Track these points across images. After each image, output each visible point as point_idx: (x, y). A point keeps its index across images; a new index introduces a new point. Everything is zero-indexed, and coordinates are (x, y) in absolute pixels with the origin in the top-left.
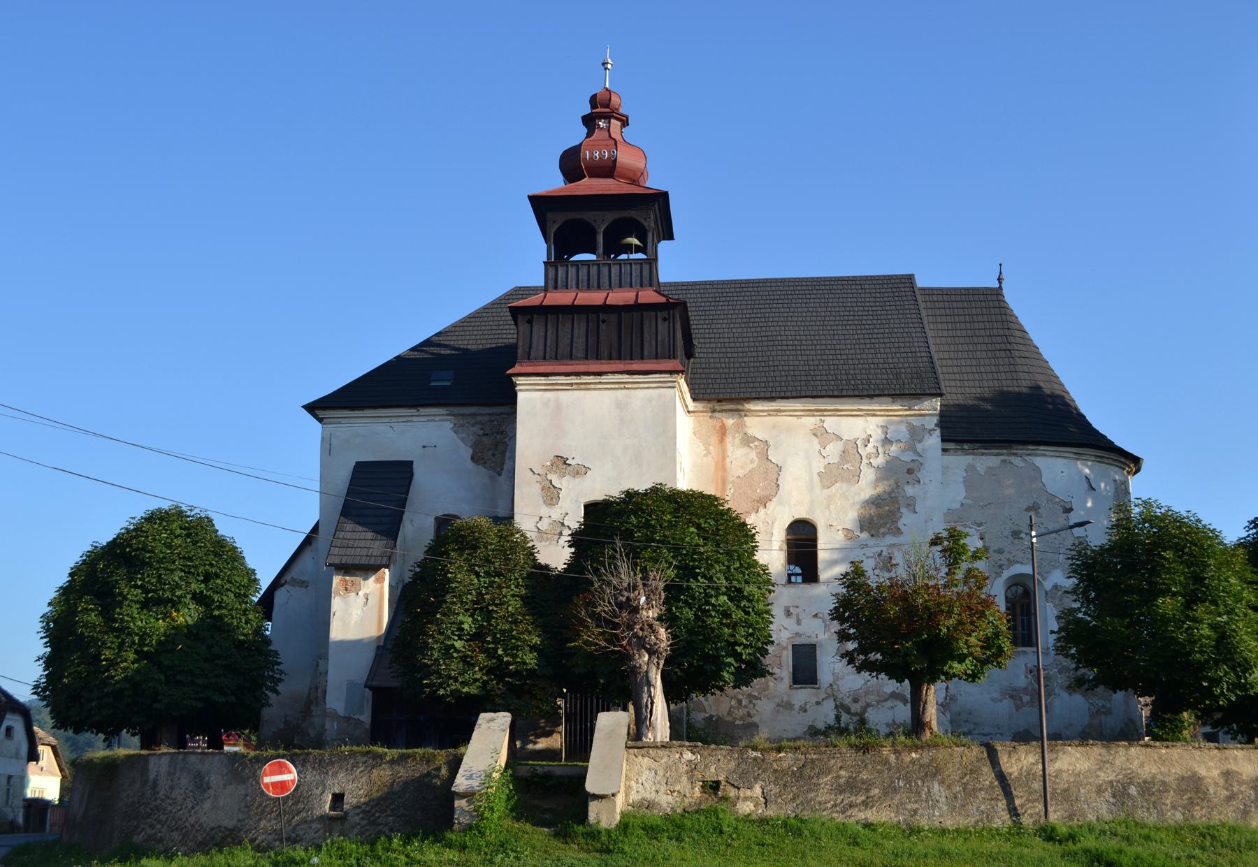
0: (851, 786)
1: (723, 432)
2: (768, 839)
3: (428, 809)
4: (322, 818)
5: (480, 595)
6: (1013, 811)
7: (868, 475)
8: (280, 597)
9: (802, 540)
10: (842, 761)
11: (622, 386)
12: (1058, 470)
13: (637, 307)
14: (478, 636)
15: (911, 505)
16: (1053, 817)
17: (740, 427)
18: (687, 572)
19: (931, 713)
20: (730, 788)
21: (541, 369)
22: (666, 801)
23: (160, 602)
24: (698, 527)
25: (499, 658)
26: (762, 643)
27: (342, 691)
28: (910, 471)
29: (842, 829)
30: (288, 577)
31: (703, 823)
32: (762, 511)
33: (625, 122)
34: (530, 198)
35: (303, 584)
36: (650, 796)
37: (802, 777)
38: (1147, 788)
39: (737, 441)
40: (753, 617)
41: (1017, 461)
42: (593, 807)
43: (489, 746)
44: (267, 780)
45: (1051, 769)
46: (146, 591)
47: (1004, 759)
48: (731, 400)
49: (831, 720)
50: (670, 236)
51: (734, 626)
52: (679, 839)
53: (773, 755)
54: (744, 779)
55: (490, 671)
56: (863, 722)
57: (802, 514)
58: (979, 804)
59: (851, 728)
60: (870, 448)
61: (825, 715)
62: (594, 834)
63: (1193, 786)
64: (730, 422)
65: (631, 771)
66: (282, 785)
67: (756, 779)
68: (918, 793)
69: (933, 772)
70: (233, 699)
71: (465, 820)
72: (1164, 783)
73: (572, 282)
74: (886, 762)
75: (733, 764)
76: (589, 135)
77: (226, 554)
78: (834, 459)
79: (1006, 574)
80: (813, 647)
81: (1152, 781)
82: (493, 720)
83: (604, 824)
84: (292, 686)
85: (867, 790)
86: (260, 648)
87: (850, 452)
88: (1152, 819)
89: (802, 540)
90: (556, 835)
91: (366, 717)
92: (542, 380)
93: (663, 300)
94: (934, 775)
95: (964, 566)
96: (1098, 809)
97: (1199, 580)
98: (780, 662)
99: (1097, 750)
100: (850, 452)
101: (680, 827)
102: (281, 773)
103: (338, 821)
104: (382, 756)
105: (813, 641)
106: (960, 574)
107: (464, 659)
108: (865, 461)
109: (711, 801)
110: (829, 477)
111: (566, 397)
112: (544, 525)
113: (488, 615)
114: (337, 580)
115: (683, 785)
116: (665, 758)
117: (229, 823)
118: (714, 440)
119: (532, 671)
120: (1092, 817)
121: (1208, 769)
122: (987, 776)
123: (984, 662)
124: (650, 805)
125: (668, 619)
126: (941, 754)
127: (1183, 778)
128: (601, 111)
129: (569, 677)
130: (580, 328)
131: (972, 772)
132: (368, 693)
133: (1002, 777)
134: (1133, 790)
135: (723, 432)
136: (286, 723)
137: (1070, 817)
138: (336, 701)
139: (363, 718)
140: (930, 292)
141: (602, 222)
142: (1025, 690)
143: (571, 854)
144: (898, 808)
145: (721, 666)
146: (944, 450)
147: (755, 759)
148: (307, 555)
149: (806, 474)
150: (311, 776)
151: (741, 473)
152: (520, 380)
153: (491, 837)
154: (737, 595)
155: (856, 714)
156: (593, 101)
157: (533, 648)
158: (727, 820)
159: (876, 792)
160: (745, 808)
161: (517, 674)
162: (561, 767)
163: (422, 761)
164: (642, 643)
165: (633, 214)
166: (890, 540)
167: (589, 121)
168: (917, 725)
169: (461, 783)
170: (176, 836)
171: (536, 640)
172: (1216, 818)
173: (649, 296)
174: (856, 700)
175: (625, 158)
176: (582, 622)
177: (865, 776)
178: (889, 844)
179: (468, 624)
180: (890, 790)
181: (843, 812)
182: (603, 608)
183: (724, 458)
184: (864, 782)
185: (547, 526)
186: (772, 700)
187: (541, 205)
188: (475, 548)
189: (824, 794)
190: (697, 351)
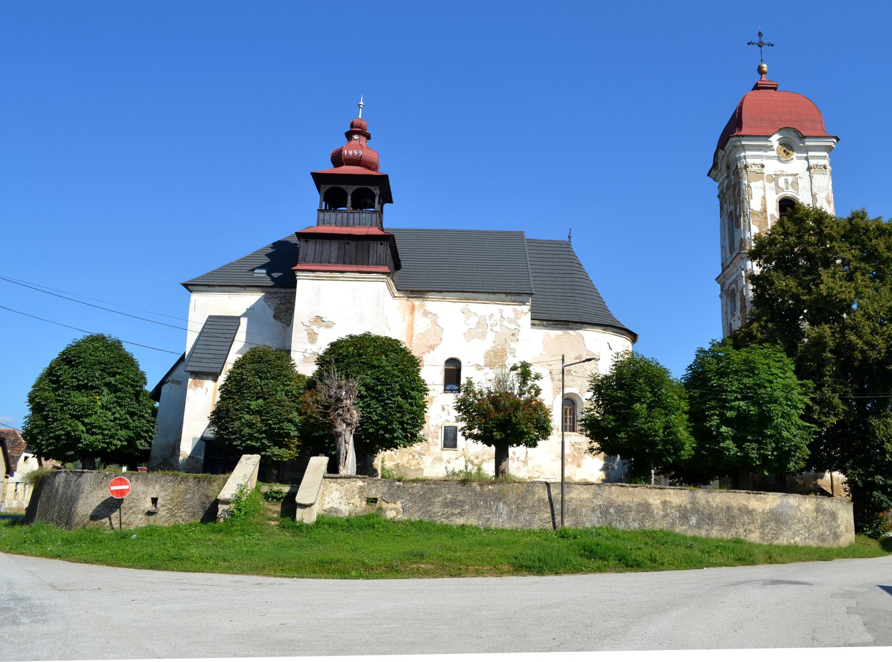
0: (453, 504)
1: (413, 308)
7: (490, 336)
8: (165, 389)
16: (566, 524)
17: (422, 306)
20: (384, 503)
22: (345, 510)
23: (86, 387)
28: (513, 335)
30: (170, 378)
33: (368, 137)
36: (336, 505)
39: (421, 314)
41: (571, 332)
42: (299, 512)
45: (567, 497)
49: (463, 468)
50: (391, 201)
56: (479, 469)
63: (646, 508)
67: (399, 498)
68: (491, 509)
70: (126, 443)
72: (629, 507)
74: (474, 490)
75: (385, 490)
78: (473, 325)
82: (249, 459)
85: (462, 506)
88: (621, 526)
91: (202, 457)
93: (382, 233)
94: (500, 499)
96: (592, 521)
102: (121, 485)
108: (489, 328)
110: (470, 335)
114: (190, 380)
118: (408, 313)
120: (588, 525)
121: (655, 500)
124: (337, 511)
127: (640, 504)
131: (523, 498)
134: (612, 510)
135: (413, 308)
137: (576, 525)
141: (350, 190)
144: (479, 517)
146: (533, 325)
147: (398, 486)
156: (352, 125)
159: (467, 507)
160: (390, 514)
172: (657, 526)
174: (477, 458)
177: (461, 498)
180: (474, 507)
181: (447, 518)
183: (413, 323)
184: (460, 502)
187: (319, 179)
189: (437, 509)
190: (403, 263)
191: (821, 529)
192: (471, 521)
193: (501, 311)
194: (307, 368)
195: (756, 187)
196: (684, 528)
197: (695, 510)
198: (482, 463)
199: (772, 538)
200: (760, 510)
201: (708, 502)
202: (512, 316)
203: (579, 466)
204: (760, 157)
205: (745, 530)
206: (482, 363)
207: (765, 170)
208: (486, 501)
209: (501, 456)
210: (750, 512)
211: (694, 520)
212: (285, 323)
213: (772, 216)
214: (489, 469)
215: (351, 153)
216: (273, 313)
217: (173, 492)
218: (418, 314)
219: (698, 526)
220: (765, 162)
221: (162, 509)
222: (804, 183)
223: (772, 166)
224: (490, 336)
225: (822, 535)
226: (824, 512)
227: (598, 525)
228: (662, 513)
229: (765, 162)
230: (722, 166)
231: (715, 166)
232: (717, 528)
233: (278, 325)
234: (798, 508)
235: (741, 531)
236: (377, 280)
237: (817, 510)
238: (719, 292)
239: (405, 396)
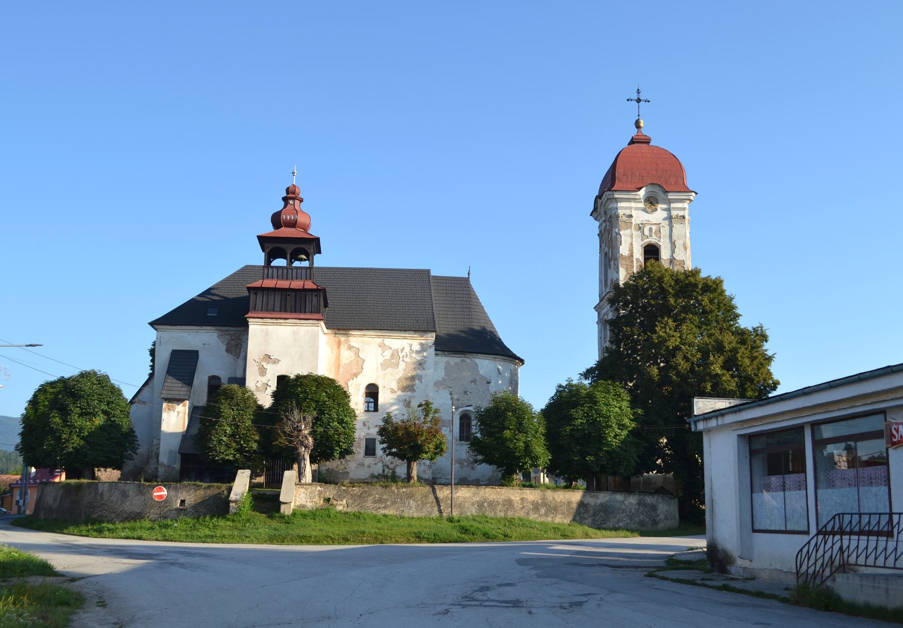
0: (380, 501)
1: (339, 343)
2: (347, 520)
3: (220, 507)
4: (176, 509)
5: (234, 418)
6: (440, 511)
7: (402, 365)
9: (372, 392)
10: (377, 491)
11: (296, 325)
12: (486, 365)
13: (304, 290)
14: (233, 436)
16: (454, 514)
17: (347, 341)
18: (321, 412)
19: (414, 473)
21: (260, 315)
22: (310, 505)
23: (88, 414)
24: (326, 392)
25: (242, 445)
26: (350, 440)
27: (167, 455)
29: (375, 516)
30: (137, 400)
31: (324, 513)
34: (258, 237)
35: (144, 403)
36: (304, 503)
37: (361, 497)
38: (491, 504)
40: (347, 431)
41: (468, 360)
42: (283, 507)
43: (242, 483)
44: (155, 494)
45: (455, 496)
46: (82, 409)
47: (438, 492)
48: (344, 329)
49: (381, 472)
50: (320, 253)
51: (339, 434)
52: (314, 519)
53: (351, 489)
54: (340, 497)
55: (237, 450)
56: (394, 472)
58: (427, 508)
59: (389, 478)
60: (404, 354)
61: (378, 469)
62: (283, 517)
63: (509, 503)
64: (343, 339)
65: (298, 492)
66: (161, 496)
69: (411, 496)
71: (234, 511)
73: (275, 276)
74: (393, 492)
76: (285, 206)
77: (116, 392)
78: (388, 357)
79: (460, 410)
83: (286, 513)
84: (142, 450)
86: (130, 435)
87: (395, 355)
89: (372, 392)
90: (268, 517)
91: (177, 466)
93: (315, 287)
95: (431, 416)
96: (472, 511)
97: (521, 424)
98: (359, 449)
99: (473, 489)
100: (395, 355)
101: (315, 515)
103: (182, 510)
104: (201, 486)
106: (429, 419)
107: (227, 445)
109: (327, 506)
110: (385, 365)
112: (259, 385)
113: (237, 427)
114: (165, 405)
115: (316, 499)
116: (310, 489)
117: (138, 511)
118: (335, 347)
119: (255, 451)
120: (469, 514)
122: (431, 498)
123: (436, 454)
124: (304, 506)
125: (313, 433)
126: (414, 489)
128: (291, 196)
129: (274, 459)
130: (278, 298)
132: (179, 456)
133: (437, 498)
134: (485, 504)
135: (339, 343)
138: (163, 459)
140: (437, 278)
142: (465, 460)
143: (274, 524)
145: (332, 450)
148: (146, 389)
149: (375, 366)
150: (172, 493)
152: (250, 320)
153: (244, 517)
154: (341, 422)
157: (256, 441)
158: (332, 512)
160: (340, 508)
161: (248, 451)
162: (268, 491)
163: (216, 488)
164: (302, 444)
165: (304, 246)
167: (285, 199)
168: (409, 477)
169: (233, 497)
170: (113, 515)
171: (257, 438)
172: (517, 515)
175: (301, 219)
176: (279, 434)
177: (385, 497)
178: (391, 522)
179: (228, 430)
182: (287, 429)
185: (261, 388)
186: (358, 464)
187: (263, 240)
188: (232, 398)
189: (369, 503)
191: (641, 517)
192: (390, 512)
193: (411, 346)
194: (266, 400)
197: (545, 504)
198: (395, 467)
204: (630, 208)
206: (396, 388)
207: (633, 220)
208: (401, 499)
211: (543, 511)
213: (638, 260)
216: (225, 347)
218: (343, 348)
222: (665, 231)
223: (639, 216)
224: (402, 365)
226: (645, 505)
227: (475, 514)
229: (634, 213)
230: (601, 210)
231: (595, 209)
232: (560, 516)
233: (229, 358)
234: (623, 502)
237: (639, 504)
239: (341, 422)
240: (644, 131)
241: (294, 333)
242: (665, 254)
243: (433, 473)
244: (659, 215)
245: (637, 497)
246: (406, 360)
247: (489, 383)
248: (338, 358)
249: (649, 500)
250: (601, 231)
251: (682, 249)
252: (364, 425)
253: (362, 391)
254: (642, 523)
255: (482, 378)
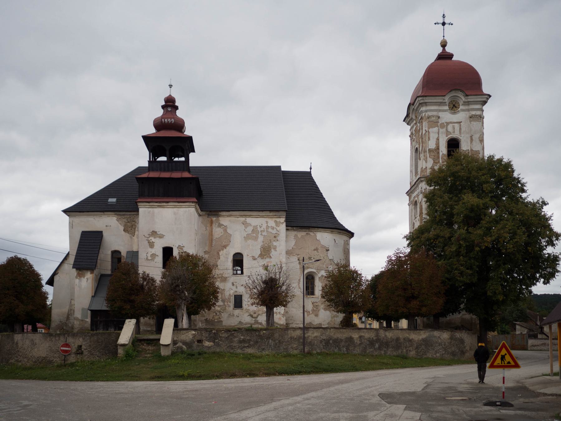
7: (261, 239)
8: (56, 278)
11: (175, 207)
12: (325, 238)
15: (275, 248)
28: (275, 237)
32: (225, 250)
41: (311, 234)
45: (306, 336)
50: (194, 151)
57: (238, 251)
64: (214, 219)
75: (207, 335)
80: (241, 296)
81: (337, 339)
85: (249, 342)
91: (89, 320)
92: (148, 204)
94: (269, 338)
100: (255, 230)
105: (241, 294)
108: (260, 233)
110: (247, 238)
111: (157, 210)
117: (44, 356)
118: (209, 225)
128: (170, 104)
134: (331, 342)
135: (212, 223)
136: (60, 322)
138: (78, 314)
139: (87, 320)
151: (218, 237)
152: (139, 204)
155: (255, 318)
159: (252, 343)
166: (268, 260)
173: (186, 175)
174: (255, 313)
183: (212, 231)
187: (147, 139)
190: (204, 193)
191: (453, 349)
193: (267, 222)
195: (433, 132)
196: (372, 350)
197: (378, 340)
199: (423, 354)
200: (416, 339)
201: (386, 336)
202: (274, 225)
203: (317, 315)
205: (407, 351)
209: (270, 314)
210: (410, 341)
212: (132, 234)
214: (263, 319)
215: (166, 120)
217: (90, 342)
219: (380, 348)
220: (441, 114)
221: (84, 351)
224: (261, 239)
225: (453, 352)
228: (359, 342)
229: (441, 114)
231: (408, 116)
233: (127, 236)
234: (439, 337)
235: (405, 351)
236: (189, 207)
237: (451, 338)
238: (408, 202)
240: (448, 49)
241: (175, 214)
242: (465, 146)
243: (286, 320)
244: (461, 116)
245: (449, 333)
246: (264, 234)
247: (328, 250)
248: (211, 234)
249: (458, 335)
250: (412, 134)
251: (478, 141)
252: (233, 285)
253: (231, 258)
254: (453, 354)
255: (323, 247)
